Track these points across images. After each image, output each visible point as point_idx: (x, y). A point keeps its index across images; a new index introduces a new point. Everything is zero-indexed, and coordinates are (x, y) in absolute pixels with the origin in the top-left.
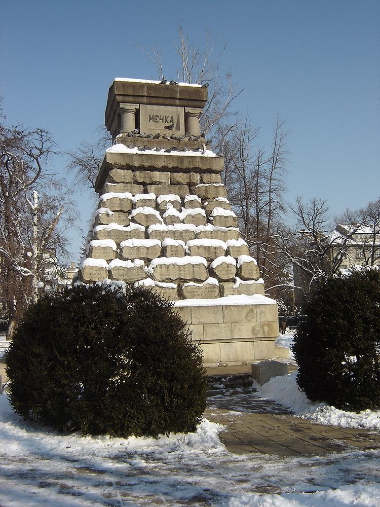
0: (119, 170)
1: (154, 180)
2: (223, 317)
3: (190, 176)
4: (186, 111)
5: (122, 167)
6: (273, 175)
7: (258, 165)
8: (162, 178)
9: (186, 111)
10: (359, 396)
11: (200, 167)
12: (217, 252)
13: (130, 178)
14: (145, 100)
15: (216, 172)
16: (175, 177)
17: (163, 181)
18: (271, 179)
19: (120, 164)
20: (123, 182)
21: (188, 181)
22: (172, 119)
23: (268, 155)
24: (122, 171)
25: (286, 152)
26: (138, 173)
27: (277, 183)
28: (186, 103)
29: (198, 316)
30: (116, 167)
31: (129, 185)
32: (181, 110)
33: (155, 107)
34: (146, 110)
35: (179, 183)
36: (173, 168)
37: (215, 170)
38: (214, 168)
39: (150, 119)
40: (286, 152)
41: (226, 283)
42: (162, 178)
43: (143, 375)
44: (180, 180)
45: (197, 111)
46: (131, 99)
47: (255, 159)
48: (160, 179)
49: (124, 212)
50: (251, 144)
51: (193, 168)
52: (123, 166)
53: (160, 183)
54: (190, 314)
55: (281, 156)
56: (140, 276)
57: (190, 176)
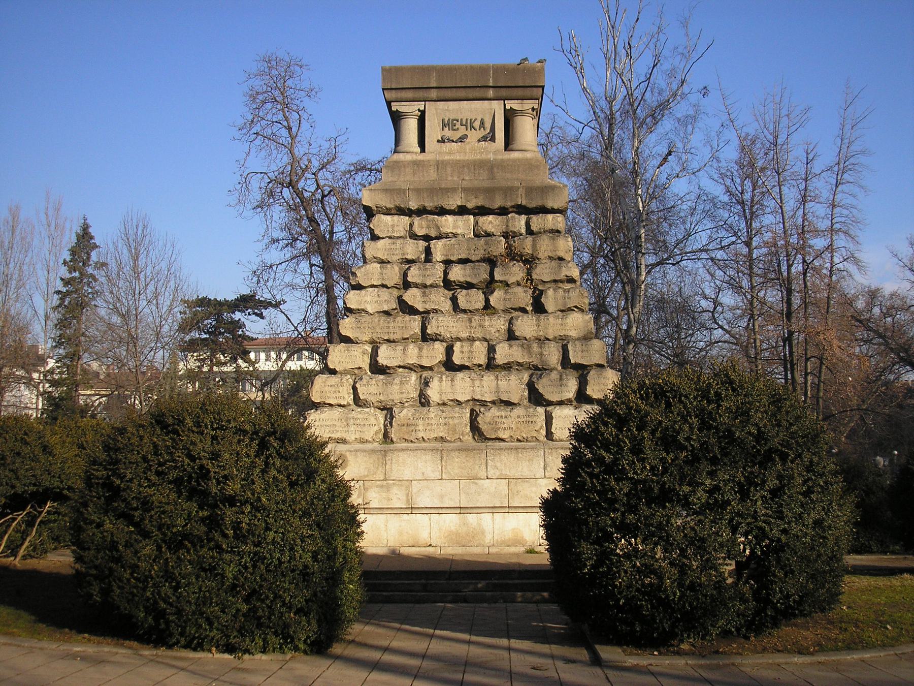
0: (383, 217)
1: (445, 230)
2: (545, 469)
3: (507, 221)
4: (508, 107)
5: (388, 212)
6: (838, 197)
7: (806, 180)
8: (458, 227)
9: (508, 107)
10: (675, 597)
11: (524, 203)
12: (545, 353)
13: (402, 229)
14: (434, 94)
15: (553, 211)
16: (480, 224)
17: (459, 231)
18: (833, 206)
19: (385, 207)
20: (390, 238)
21: (504, 228)
22: (482, 123)
23: (826, 157)
24: (389, 218)
25: (863, 152)
26: (417, 221)
27: (845, 212)
28: (504, 93)
29: (498, 464)
30: (379, 212)
31: (399, 241)
32: (497, 107)
33: (452, 105)
34: (436, 113)
35: (488, 235)
36: (477, 207)
37: (553, 209)
38: (550, 204)
39: (444, 125)
40: (863, 152)
41: (558, 407)
42: (458, 227)
43: (165, 527)
44: (490, 229)
45: (529, 105)
46: (409, 94)
47: (800, 168)
48: (454, 227)
49: (388, 288)
50: (795, 139)
51: (513, 207)
52: (390, 209)
53: (455, 235)
54: (484, 462)
55: (852, 160)
56: (404, 396)
57: (507, 221)
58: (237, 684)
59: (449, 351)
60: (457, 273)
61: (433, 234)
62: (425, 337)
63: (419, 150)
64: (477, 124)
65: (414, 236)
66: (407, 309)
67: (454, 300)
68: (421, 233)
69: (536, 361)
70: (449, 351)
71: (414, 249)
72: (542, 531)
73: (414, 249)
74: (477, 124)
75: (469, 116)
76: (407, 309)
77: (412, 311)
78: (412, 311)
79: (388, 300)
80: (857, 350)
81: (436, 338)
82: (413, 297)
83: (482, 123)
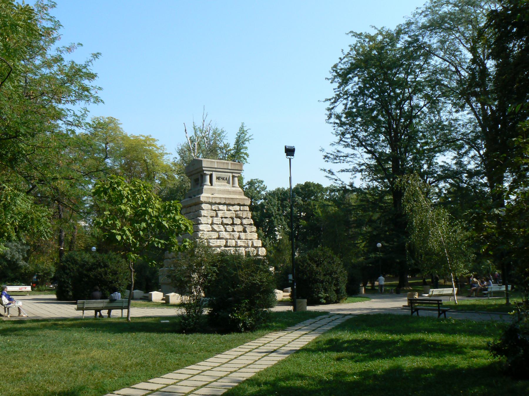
22: (226, 178)
58: (122, 395)
59: (227, 242)
60: (225, 221)
61: (217, 209)
62: (219, 238)
63: (210, 184)
64: (225, 179)
65: (212, 210)
66: (213, 230)
67: (225, 228)
68: (214, 209)
69: (246, 245)
70: (227, 242)
71: (214, 214)
72: (303, 183)
73: (214, 214)
74: (225, 179)
75: (224, 176)
76: (213, 230)
77: (215, 231)
78: (215, 231)
79: (209, 227)
80: (138, 196)
81: (222, 238)
82: (215, 227)
83: (226, 178)
